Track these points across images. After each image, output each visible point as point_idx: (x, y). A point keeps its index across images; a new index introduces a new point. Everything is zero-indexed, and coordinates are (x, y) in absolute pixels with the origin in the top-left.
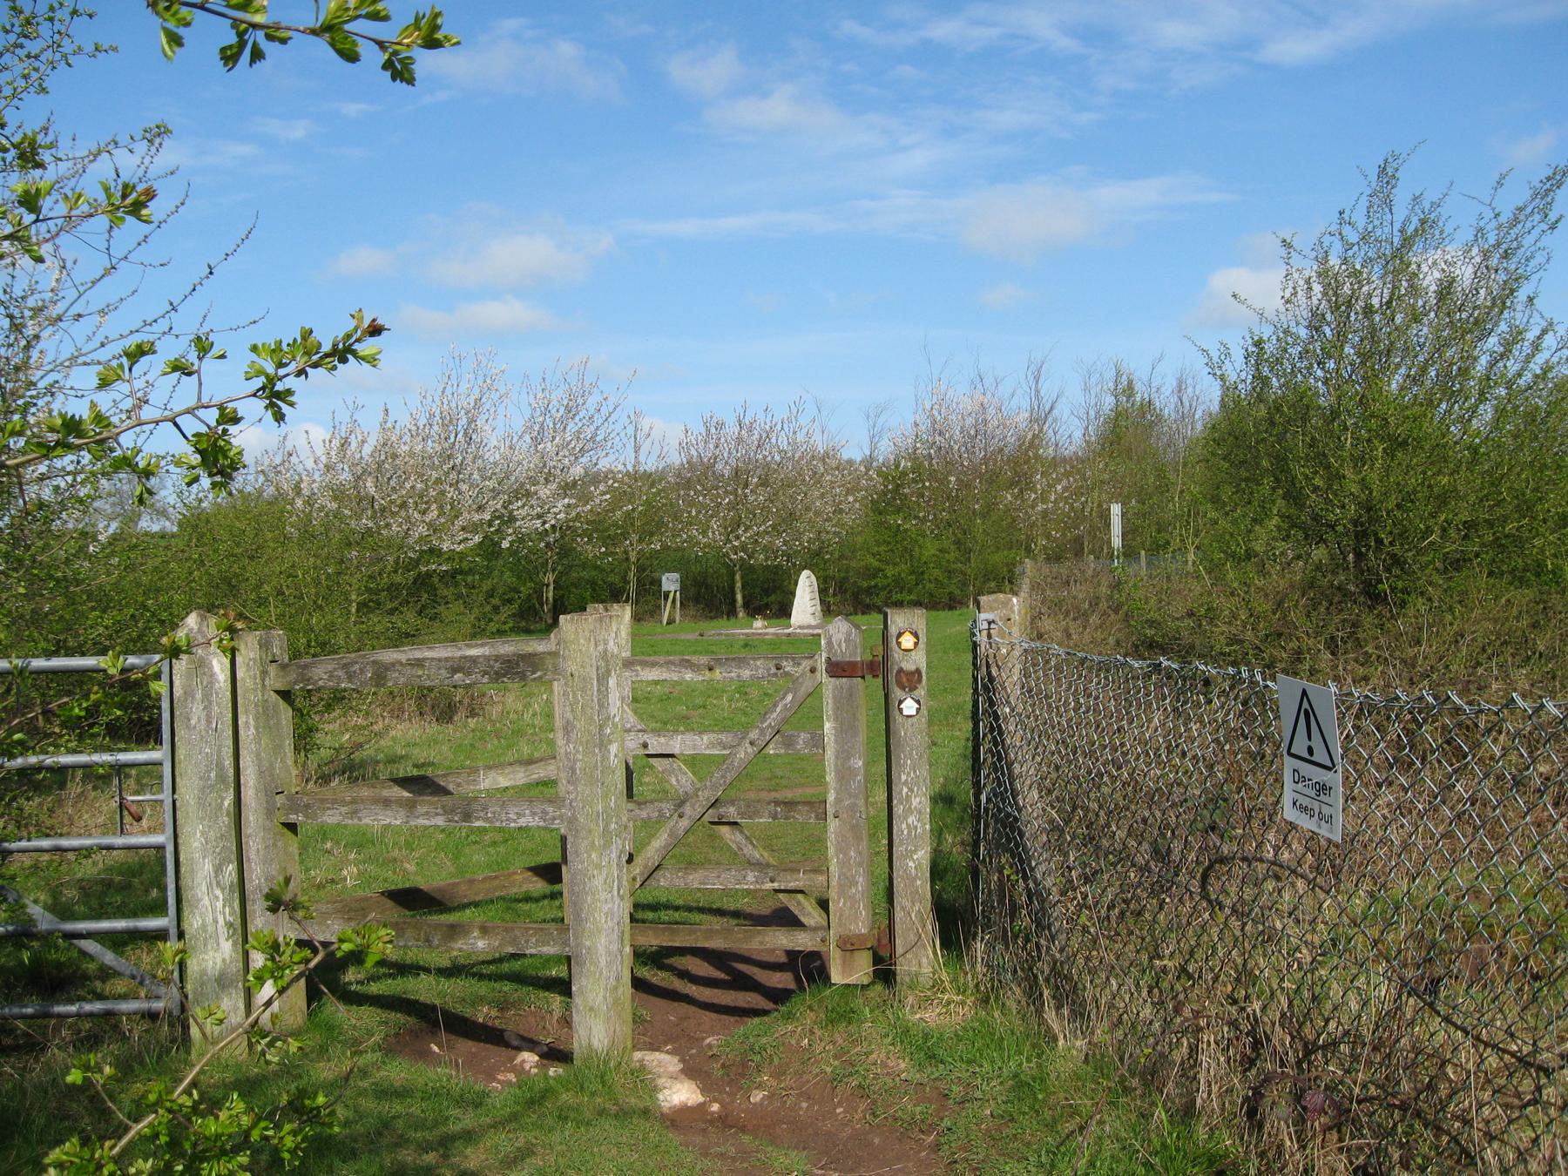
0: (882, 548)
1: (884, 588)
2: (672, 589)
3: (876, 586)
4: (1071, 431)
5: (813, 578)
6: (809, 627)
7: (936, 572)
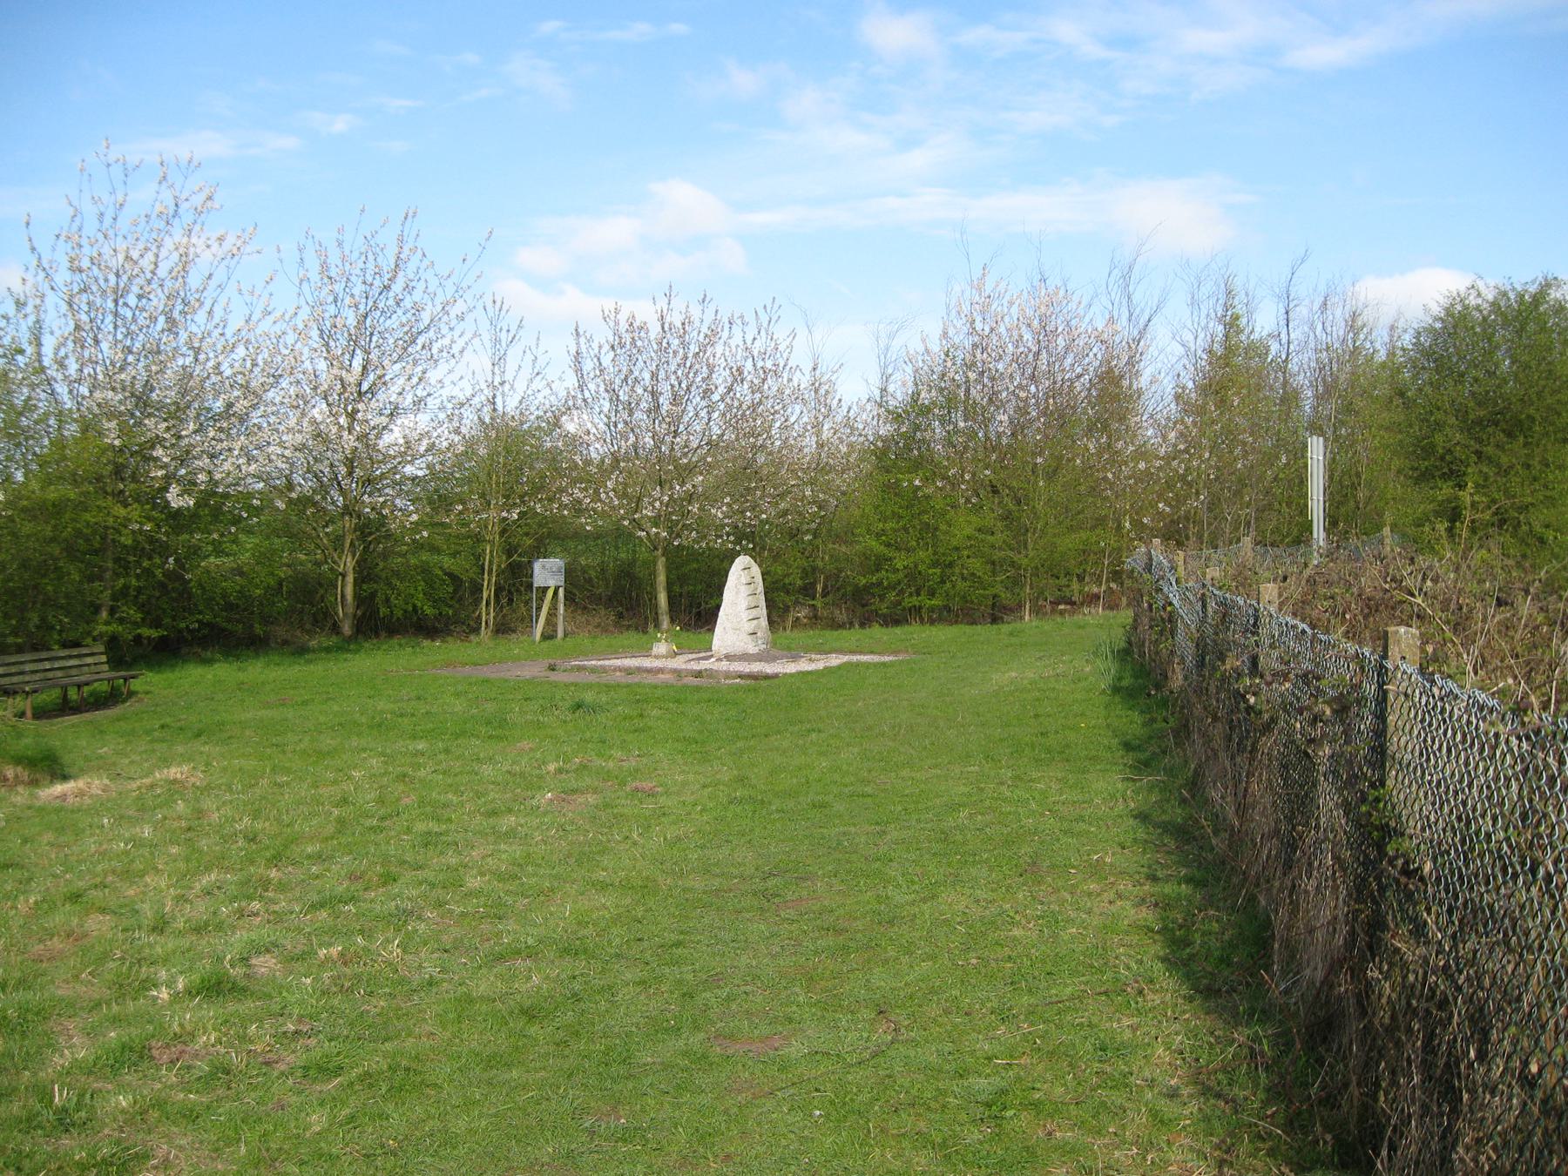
0: (890, 525)
1: (892, 587)
2: (552, 583)
3: (880, 583)
4: (1166, 368)
5: (756, 571)
6: (745, 657)
7: (976, 565)
